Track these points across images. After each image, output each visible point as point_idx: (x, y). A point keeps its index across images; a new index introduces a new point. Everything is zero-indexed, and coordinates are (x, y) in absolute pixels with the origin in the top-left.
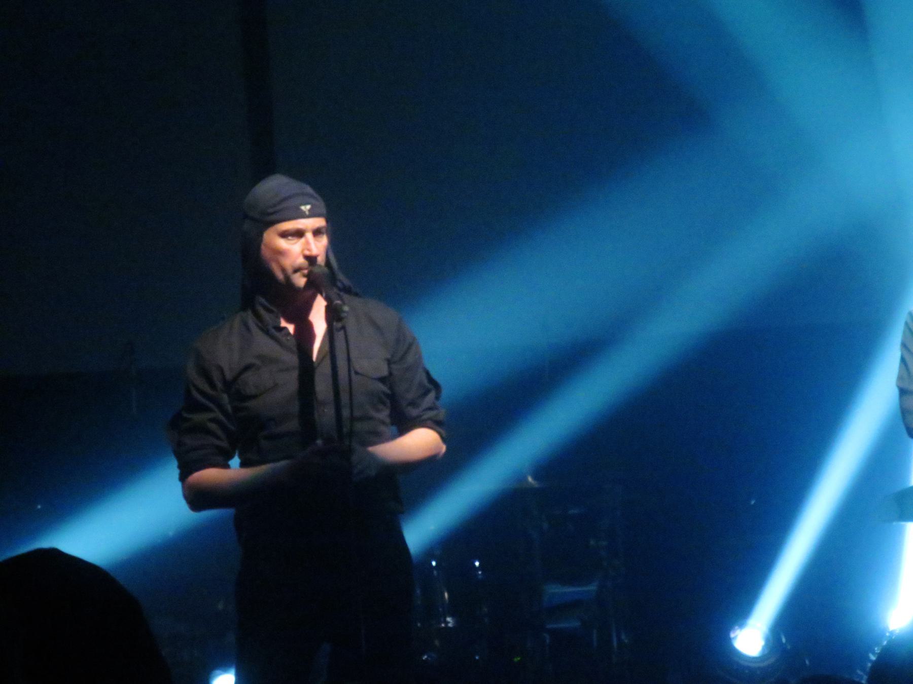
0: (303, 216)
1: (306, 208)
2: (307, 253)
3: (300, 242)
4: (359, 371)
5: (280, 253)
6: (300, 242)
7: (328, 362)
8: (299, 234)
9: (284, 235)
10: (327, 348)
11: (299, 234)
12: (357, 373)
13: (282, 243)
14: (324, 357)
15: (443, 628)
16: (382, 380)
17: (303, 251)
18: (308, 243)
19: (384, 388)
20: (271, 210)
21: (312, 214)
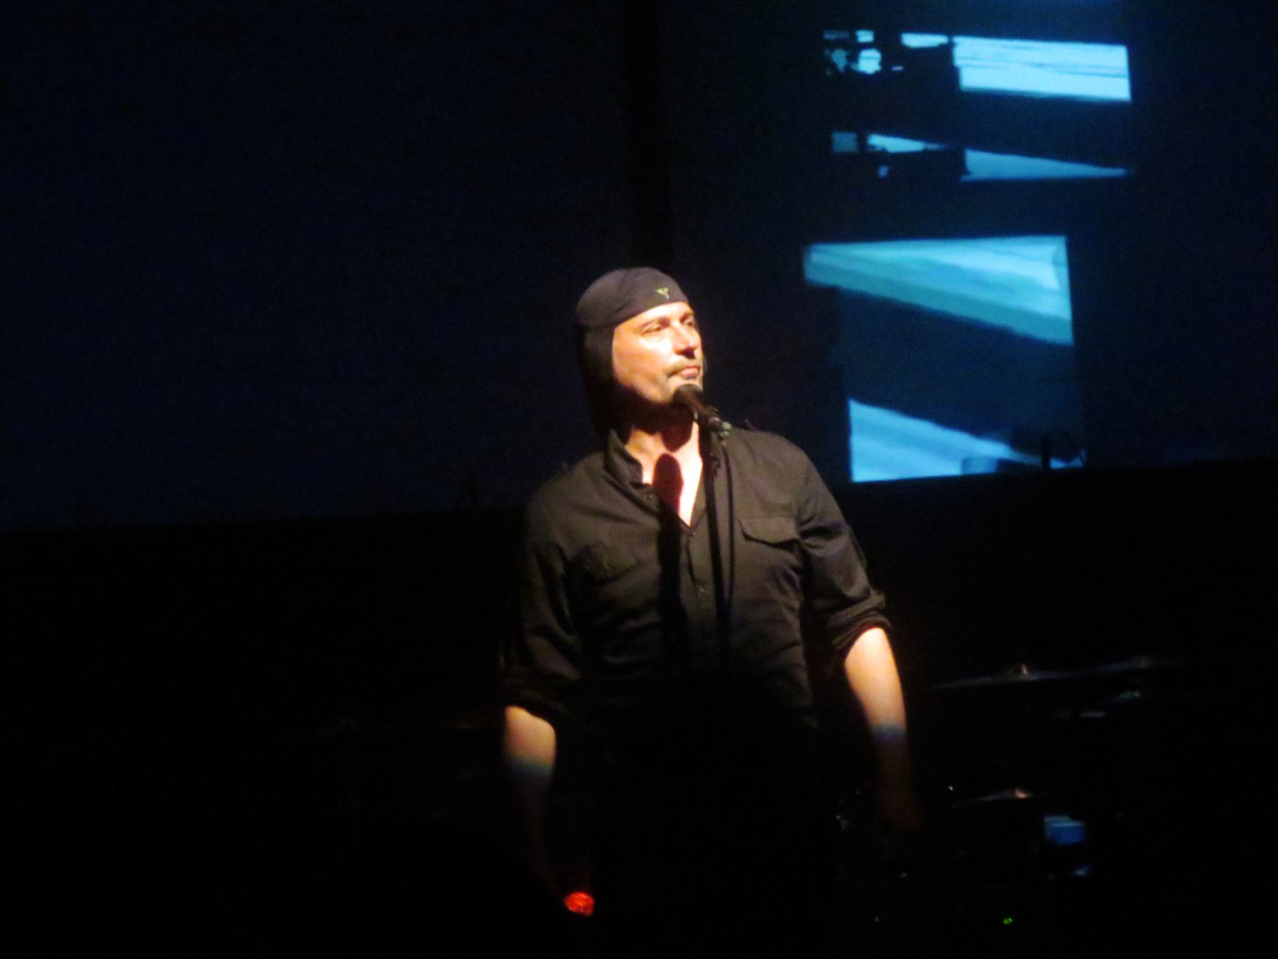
0: (661, 301)
1: (663, 291)
2: (682, 347)
3: (659, 343)
4: (750, 532)
5: (642, 355)
6: (659, 343)
7: (704, 528)
8: (664, 323)
9: (645, 331)
10: (703, 505)
11: (664, 323)
12: (748, 538)
13: (648, 344)
14: (701, 518)
15: (847, 157)
16: (787, 545)
17: (674, 347)
18: (678, 334)
19: (792, 558)
20: (618, 306)
21: (673, 300)
